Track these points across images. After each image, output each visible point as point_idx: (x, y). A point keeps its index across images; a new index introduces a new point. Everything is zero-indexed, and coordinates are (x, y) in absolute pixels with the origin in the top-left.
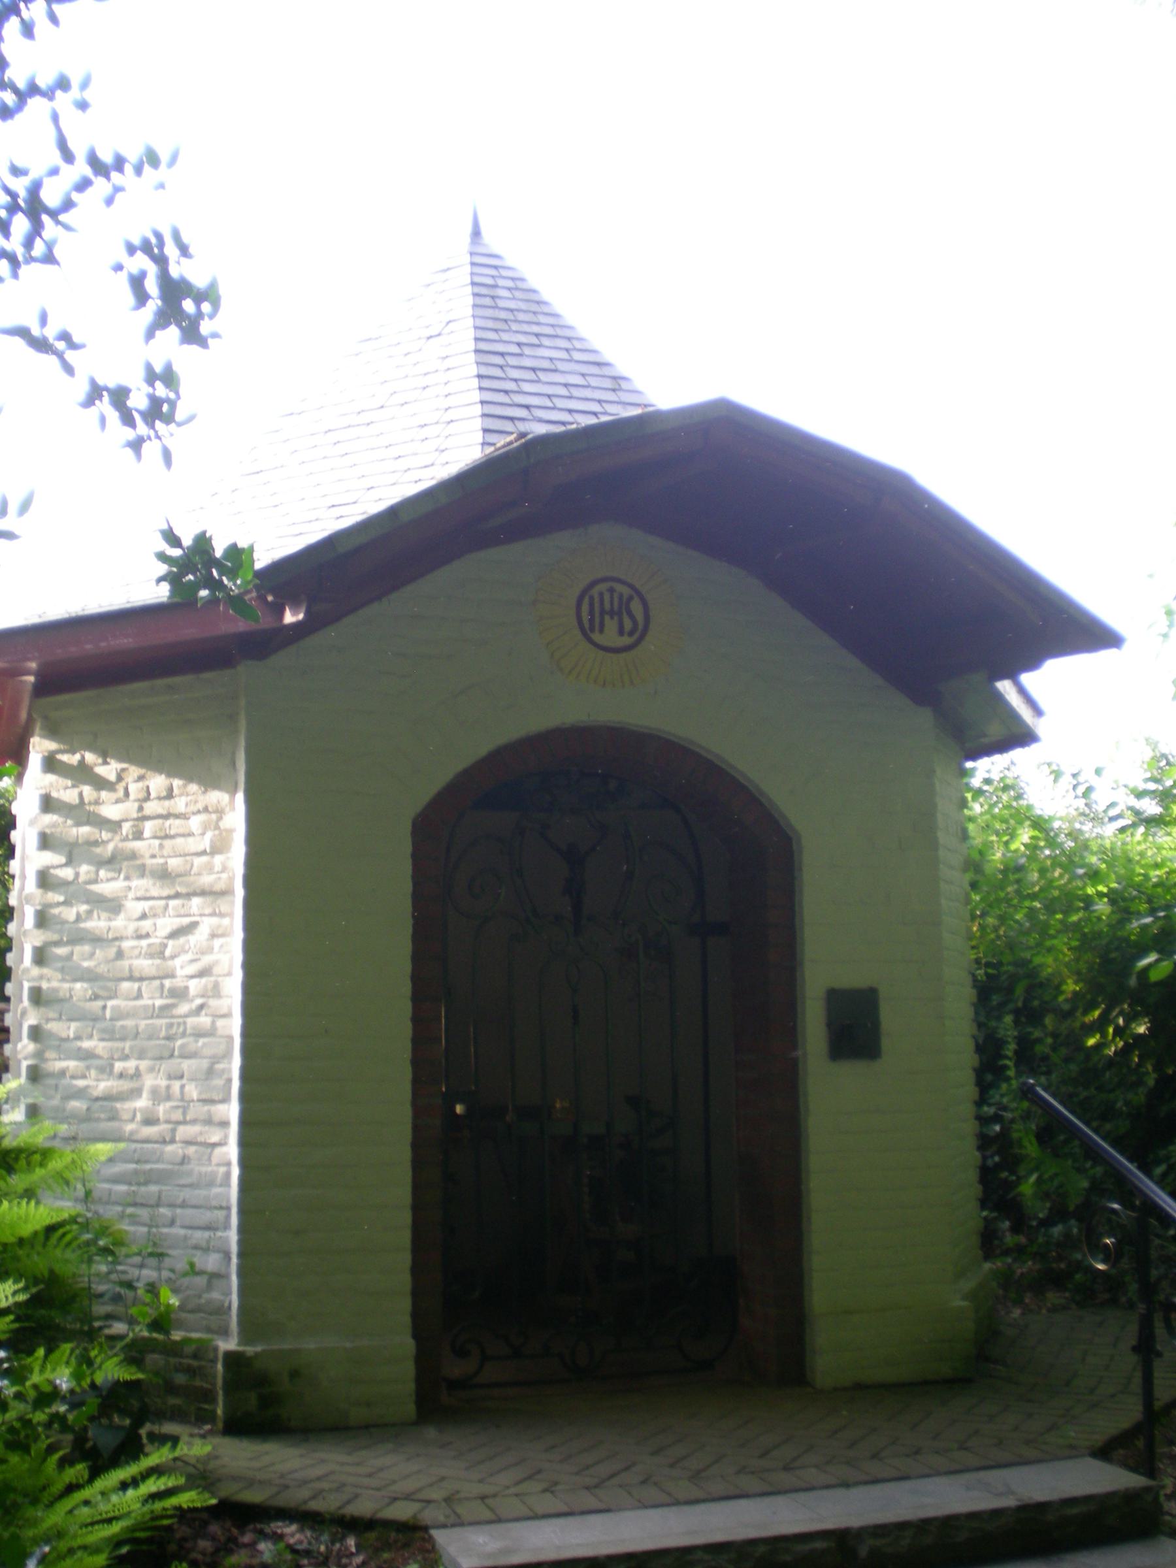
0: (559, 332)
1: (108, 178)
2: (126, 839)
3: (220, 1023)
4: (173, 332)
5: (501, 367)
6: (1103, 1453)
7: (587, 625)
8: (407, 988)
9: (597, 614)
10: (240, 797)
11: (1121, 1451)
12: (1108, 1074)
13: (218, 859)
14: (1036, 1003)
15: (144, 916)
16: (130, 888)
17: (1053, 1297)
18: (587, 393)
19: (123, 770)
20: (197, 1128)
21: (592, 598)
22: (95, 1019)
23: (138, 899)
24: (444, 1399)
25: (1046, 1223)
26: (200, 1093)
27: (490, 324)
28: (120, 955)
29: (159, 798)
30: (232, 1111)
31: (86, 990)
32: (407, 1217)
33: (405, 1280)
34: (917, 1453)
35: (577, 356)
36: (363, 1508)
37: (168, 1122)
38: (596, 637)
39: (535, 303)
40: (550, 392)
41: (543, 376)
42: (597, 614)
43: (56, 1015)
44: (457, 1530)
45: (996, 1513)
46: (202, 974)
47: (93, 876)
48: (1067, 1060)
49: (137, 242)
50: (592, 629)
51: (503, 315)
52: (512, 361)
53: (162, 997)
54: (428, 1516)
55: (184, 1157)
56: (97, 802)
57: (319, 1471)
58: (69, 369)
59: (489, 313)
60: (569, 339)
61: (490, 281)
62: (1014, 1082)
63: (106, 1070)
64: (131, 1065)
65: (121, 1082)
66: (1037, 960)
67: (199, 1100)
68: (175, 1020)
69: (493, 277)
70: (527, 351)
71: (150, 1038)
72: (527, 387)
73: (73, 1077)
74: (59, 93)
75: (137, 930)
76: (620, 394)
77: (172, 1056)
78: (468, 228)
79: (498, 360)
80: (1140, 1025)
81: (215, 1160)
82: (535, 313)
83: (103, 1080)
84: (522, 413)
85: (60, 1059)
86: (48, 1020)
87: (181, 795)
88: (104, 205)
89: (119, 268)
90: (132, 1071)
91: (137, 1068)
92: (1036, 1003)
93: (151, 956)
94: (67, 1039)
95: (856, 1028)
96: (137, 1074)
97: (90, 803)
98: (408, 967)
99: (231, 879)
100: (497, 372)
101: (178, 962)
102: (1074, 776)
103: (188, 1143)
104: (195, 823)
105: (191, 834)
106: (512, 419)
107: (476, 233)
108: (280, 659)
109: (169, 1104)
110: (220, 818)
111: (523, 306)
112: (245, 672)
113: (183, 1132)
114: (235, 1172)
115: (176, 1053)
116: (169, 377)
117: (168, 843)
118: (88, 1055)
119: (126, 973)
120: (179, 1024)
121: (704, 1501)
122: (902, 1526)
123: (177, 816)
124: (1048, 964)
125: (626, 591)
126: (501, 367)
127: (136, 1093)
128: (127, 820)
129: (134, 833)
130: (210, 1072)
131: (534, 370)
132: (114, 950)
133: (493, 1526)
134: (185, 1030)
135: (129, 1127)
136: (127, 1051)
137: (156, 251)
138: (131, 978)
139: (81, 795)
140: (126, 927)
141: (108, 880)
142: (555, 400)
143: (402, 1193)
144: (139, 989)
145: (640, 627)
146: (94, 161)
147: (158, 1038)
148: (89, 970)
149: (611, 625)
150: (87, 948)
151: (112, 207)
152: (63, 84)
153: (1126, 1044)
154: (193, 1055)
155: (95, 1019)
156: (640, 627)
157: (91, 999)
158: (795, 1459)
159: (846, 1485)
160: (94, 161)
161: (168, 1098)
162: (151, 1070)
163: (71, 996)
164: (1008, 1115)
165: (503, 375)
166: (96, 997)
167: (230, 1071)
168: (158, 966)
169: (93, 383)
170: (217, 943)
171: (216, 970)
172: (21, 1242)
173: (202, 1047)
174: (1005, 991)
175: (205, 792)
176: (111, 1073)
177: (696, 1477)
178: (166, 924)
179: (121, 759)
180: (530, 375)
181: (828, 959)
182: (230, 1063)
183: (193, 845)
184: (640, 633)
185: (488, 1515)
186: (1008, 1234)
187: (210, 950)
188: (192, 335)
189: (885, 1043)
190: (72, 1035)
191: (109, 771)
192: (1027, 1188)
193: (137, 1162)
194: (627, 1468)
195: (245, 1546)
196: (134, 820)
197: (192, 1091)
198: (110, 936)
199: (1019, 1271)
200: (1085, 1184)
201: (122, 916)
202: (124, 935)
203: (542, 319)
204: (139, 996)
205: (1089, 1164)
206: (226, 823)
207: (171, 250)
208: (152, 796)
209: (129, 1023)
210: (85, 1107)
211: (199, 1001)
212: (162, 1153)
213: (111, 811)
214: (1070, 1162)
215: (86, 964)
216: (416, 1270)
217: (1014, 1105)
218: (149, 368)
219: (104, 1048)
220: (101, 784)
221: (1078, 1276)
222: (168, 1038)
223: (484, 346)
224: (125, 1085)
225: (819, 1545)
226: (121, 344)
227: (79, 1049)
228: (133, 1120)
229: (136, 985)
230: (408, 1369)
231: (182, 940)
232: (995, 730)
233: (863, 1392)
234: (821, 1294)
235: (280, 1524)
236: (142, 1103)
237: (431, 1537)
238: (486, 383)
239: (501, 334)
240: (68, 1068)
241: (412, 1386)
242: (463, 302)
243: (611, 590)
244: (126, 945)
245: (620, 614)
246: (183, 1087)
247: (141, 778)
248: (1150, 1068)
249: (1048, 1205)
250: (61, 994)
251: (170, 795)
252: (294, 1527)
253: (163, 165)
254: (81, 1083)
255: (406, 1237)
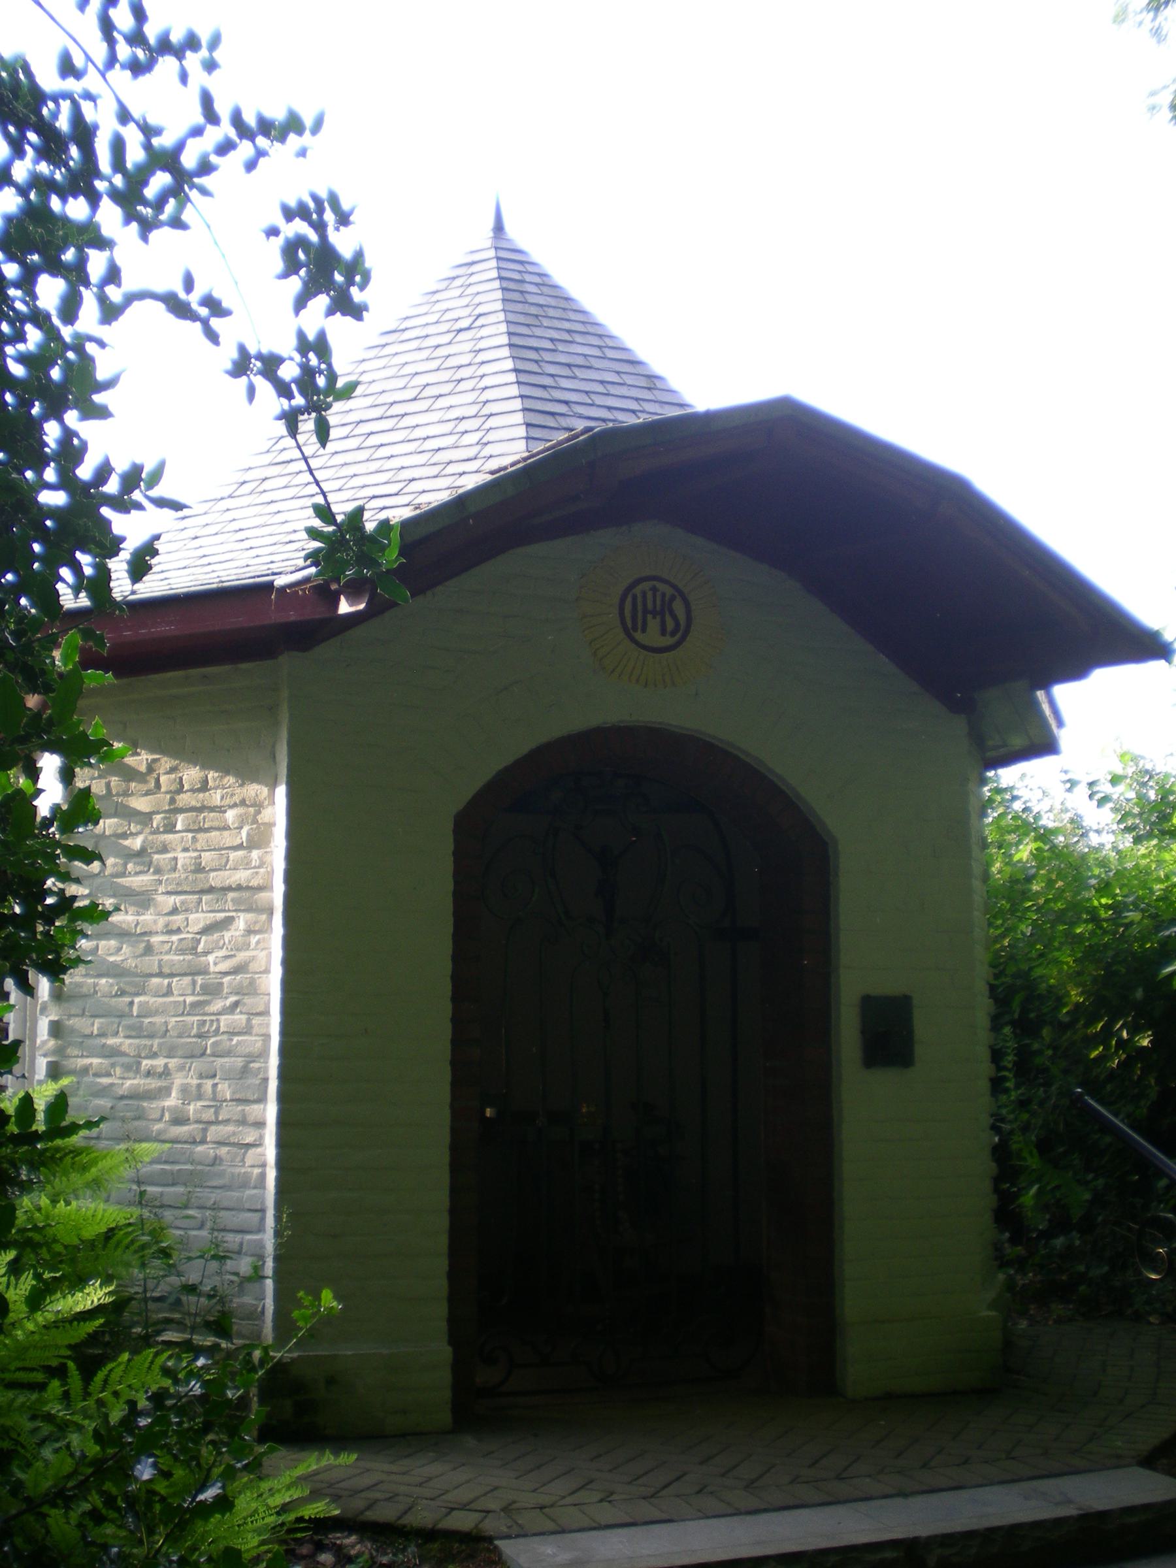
0: (591, 329)
1: (253, 141)
2: (156, 832)
3: (256, 1021)
4: (322, 301)
5: (536, 362)
6: (1148, 1461)
7: (630, 625)
8: (447, 988)
9: (640, 615)
10: (281, 791)
11: (1165, 1461)
12: (1109, 1087)
13: (255, 854)
14: (1032, 1015)
15: (174, 911)
16: (160, 882)
17: (1058, 1309)
18: (623, 391)
19: (154, 761)
20: (230, 1128)
21: (635, 598)
22: (122, 1016)
23: (168, 893)
24: (480, 1409)
25: (1047, 1235)
26: (233, 1093)
27: (522, 319)
28: (149, 950)
29: (193, 791)
30: (271, 1112)
31: (112, 985)
32: (444, 1222)
33: (441, 1285)
34: (965, 1462)
35: (610, 354)
36: (423, 1517)
37: (198, 1122)
38: (638, 636)
39: (564, 302)
40: (587, 389)
41: (579, 373)
42: (640, 615)
43: (79, 1012)
44: (521, 1540)
45: (1058, 1522)
46: (236, 971)
47: (120, 869)
48: (1066, 1072)
49: (293, 204)
50: (635, 629)
51: (534, 310)
52: (548, 357)
53: (193, 994)
54: (490, 1526)
55: (216, 1157)
56: (126, 793)
57: (367, 1480)
58: (212, 337)
59: (519, 307)
60: (600, 336)
61: (517, 276)
62: (1013, 1093)
63: (133, 1068)
64: (160, 1062)
65: (148, 1081)
66: (1039, 972)
67: (232, 1100)
68: (207, 1018)
69: (520, 272)
70: (561, 347)
71: (180, 1036)
72: (565, 383)
73: (96, 1075)
74: (188, 54)
75: (167, 925)
76: (655, 392)
77: (203, 1054)
78: (490, 223)
79: (532, 355)
80: (1144, 1038)
81: (248, 1162)
82: (564, 309)
83: (130, 1079)
84: (562, 409)
85: (82, 1056)
86: (70, 1016)
87: (216, 788)
88: (243, 170)
89: (273, 232)
90: (160, 1070)
91: (166, 1065)
92: (1032, 1015)
93: (182, 951)
94: (91, 1036)
95: (890, 1035)
96: (166, 1073)
97: (118, 795)
98: (448, 966)
99: (271, 874)
100: (534, 367)
101: (211, 958)
102: (1091, 784)
103: (220, 1143)
104: (231, 815)
105: (226, 828)
106: (553, 414)
107: (499, 228)
108: (322, 651)
109: (200, 1104)
110: (259, 812)
111: (552, 302)
112: (287, 662)
113: (214, 1132)
114: (271, 1175)
115: (208, 1051)
116: (321, 346)
117: (200, 836)
118: (114, 1052)
119: (156, 970)
120: (212, 1021)
121: (765, 1510)
122: (970, 1535)
123: (212, 809)
124: (1050, 976)
125: (669, 591)
126: (536, 362)
127: (165, 1092)
128: (158, 813)
129: (165, 825)
130: (245, 1071)
131: (569, 366)
132: (143, 945)
133: (559, 1537)
134: (218, 1028)
135: (157, 1127)
136: (155, 1048)
137: (315, 216)
138: (160, 974)
139: (108, 785)
140: (155, 922)
141: (137, 874)
142: (593, 396)
143: (441, 1197)
144: (169, 985)
145: (682, 627)
146: (237, 120)
147: (189, 1036)
148: (114, 965)
149: (653, 624)
150: (113, 943)
151: (254, 172)
152: (192, 42)
153: (1129, 1057)
154: (228, 1053)
155: (122, 1016)
156: (682, 627)
157: (116, 995)
158: (846, 1469)
159: (904, 1495)
160: (237, 120)
161: (200, 1097)
162: (181, 1068)
163: (96, 992)
164: (1006, 1127)
165: (539, 371)
166: (123, 993)
167: (266, 1070)
168: (189, 961)
169: (242, 349)
170: (254, 939)
171: (253, 967)
172: (91, 1244)
173: (237, 1045)
174: (1017, 1001)
175: (242, 785)
176: (138, 1071)
177: (750, 1486)
178: (198, 920)
179: (152, 750)
180: (565, 372)
181: (862, 966)
182: (266, 1062)
183: (228, 839)
184: (682, 632)
185: (550, 1526)
186: (1006, 1245)
187: (247, 946)
188: (345, 306)
189: (919, 1050)
190: (95, 1032)
191: (140, 760)
192: (1029, 1198)
193: (166, 1162)
194: (678, 1479)
195: (304, 1557)
196: (165, 812)
197: (226, 1090)
198: (138, 931)
199: (1021, 1282)
200: (1087, 1196)
201: (152, 910)
202: (154, 928)
203: (572, 316)
204: (169, 992)
205: (1090, 1176)
206: (265, 816)
207: (329, 217)
208: (186, 788)
209: (158, 1020)
210: (110, 1105)
211: (233, 999)
212: (192, 1153)
213: (140, 804)
214: (1070, 1174)
215: (111, 959)
216: (453, 1275)
217: (1012, 1116)
218: (301, 335)
219: (130, 1045)
220: (130, 774)
221: (1082, 1288)
222: (199, 1036)
223: (517, 341)
224: (153, 1084)
225: (889, 1554)
226: (270, 313)
227: (104, 1045)
228: (160, 1119)
229: (166, 981)
230: (445, 1376)
231: (216, 936)
232: (1017, 742)
233: (891, 1401)
234: (853, 1302)
235: (339, 1535)
236: (172, 1101)
237: (496, 1547)
238: (524, 378)
239: (534, 329)
240: (91, 1064)
241: (447, 1394)
242: (492, 300)
243: (654, 590)
244: (155, 939)
245: (662, 613)
246: (215, 1085)
247: (173, 770)
248: (1153, 1082)
249: (1047, 1217)
250: (84, 990)
251: (204, 787)
252: (353, 1538)
253: (307, 133)
254: (105, 1081)
255: (443, 1241)
